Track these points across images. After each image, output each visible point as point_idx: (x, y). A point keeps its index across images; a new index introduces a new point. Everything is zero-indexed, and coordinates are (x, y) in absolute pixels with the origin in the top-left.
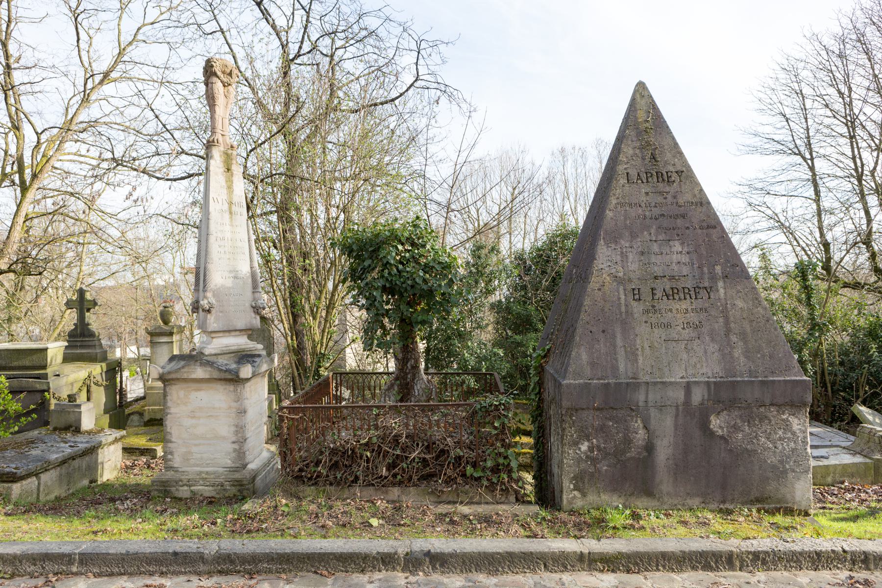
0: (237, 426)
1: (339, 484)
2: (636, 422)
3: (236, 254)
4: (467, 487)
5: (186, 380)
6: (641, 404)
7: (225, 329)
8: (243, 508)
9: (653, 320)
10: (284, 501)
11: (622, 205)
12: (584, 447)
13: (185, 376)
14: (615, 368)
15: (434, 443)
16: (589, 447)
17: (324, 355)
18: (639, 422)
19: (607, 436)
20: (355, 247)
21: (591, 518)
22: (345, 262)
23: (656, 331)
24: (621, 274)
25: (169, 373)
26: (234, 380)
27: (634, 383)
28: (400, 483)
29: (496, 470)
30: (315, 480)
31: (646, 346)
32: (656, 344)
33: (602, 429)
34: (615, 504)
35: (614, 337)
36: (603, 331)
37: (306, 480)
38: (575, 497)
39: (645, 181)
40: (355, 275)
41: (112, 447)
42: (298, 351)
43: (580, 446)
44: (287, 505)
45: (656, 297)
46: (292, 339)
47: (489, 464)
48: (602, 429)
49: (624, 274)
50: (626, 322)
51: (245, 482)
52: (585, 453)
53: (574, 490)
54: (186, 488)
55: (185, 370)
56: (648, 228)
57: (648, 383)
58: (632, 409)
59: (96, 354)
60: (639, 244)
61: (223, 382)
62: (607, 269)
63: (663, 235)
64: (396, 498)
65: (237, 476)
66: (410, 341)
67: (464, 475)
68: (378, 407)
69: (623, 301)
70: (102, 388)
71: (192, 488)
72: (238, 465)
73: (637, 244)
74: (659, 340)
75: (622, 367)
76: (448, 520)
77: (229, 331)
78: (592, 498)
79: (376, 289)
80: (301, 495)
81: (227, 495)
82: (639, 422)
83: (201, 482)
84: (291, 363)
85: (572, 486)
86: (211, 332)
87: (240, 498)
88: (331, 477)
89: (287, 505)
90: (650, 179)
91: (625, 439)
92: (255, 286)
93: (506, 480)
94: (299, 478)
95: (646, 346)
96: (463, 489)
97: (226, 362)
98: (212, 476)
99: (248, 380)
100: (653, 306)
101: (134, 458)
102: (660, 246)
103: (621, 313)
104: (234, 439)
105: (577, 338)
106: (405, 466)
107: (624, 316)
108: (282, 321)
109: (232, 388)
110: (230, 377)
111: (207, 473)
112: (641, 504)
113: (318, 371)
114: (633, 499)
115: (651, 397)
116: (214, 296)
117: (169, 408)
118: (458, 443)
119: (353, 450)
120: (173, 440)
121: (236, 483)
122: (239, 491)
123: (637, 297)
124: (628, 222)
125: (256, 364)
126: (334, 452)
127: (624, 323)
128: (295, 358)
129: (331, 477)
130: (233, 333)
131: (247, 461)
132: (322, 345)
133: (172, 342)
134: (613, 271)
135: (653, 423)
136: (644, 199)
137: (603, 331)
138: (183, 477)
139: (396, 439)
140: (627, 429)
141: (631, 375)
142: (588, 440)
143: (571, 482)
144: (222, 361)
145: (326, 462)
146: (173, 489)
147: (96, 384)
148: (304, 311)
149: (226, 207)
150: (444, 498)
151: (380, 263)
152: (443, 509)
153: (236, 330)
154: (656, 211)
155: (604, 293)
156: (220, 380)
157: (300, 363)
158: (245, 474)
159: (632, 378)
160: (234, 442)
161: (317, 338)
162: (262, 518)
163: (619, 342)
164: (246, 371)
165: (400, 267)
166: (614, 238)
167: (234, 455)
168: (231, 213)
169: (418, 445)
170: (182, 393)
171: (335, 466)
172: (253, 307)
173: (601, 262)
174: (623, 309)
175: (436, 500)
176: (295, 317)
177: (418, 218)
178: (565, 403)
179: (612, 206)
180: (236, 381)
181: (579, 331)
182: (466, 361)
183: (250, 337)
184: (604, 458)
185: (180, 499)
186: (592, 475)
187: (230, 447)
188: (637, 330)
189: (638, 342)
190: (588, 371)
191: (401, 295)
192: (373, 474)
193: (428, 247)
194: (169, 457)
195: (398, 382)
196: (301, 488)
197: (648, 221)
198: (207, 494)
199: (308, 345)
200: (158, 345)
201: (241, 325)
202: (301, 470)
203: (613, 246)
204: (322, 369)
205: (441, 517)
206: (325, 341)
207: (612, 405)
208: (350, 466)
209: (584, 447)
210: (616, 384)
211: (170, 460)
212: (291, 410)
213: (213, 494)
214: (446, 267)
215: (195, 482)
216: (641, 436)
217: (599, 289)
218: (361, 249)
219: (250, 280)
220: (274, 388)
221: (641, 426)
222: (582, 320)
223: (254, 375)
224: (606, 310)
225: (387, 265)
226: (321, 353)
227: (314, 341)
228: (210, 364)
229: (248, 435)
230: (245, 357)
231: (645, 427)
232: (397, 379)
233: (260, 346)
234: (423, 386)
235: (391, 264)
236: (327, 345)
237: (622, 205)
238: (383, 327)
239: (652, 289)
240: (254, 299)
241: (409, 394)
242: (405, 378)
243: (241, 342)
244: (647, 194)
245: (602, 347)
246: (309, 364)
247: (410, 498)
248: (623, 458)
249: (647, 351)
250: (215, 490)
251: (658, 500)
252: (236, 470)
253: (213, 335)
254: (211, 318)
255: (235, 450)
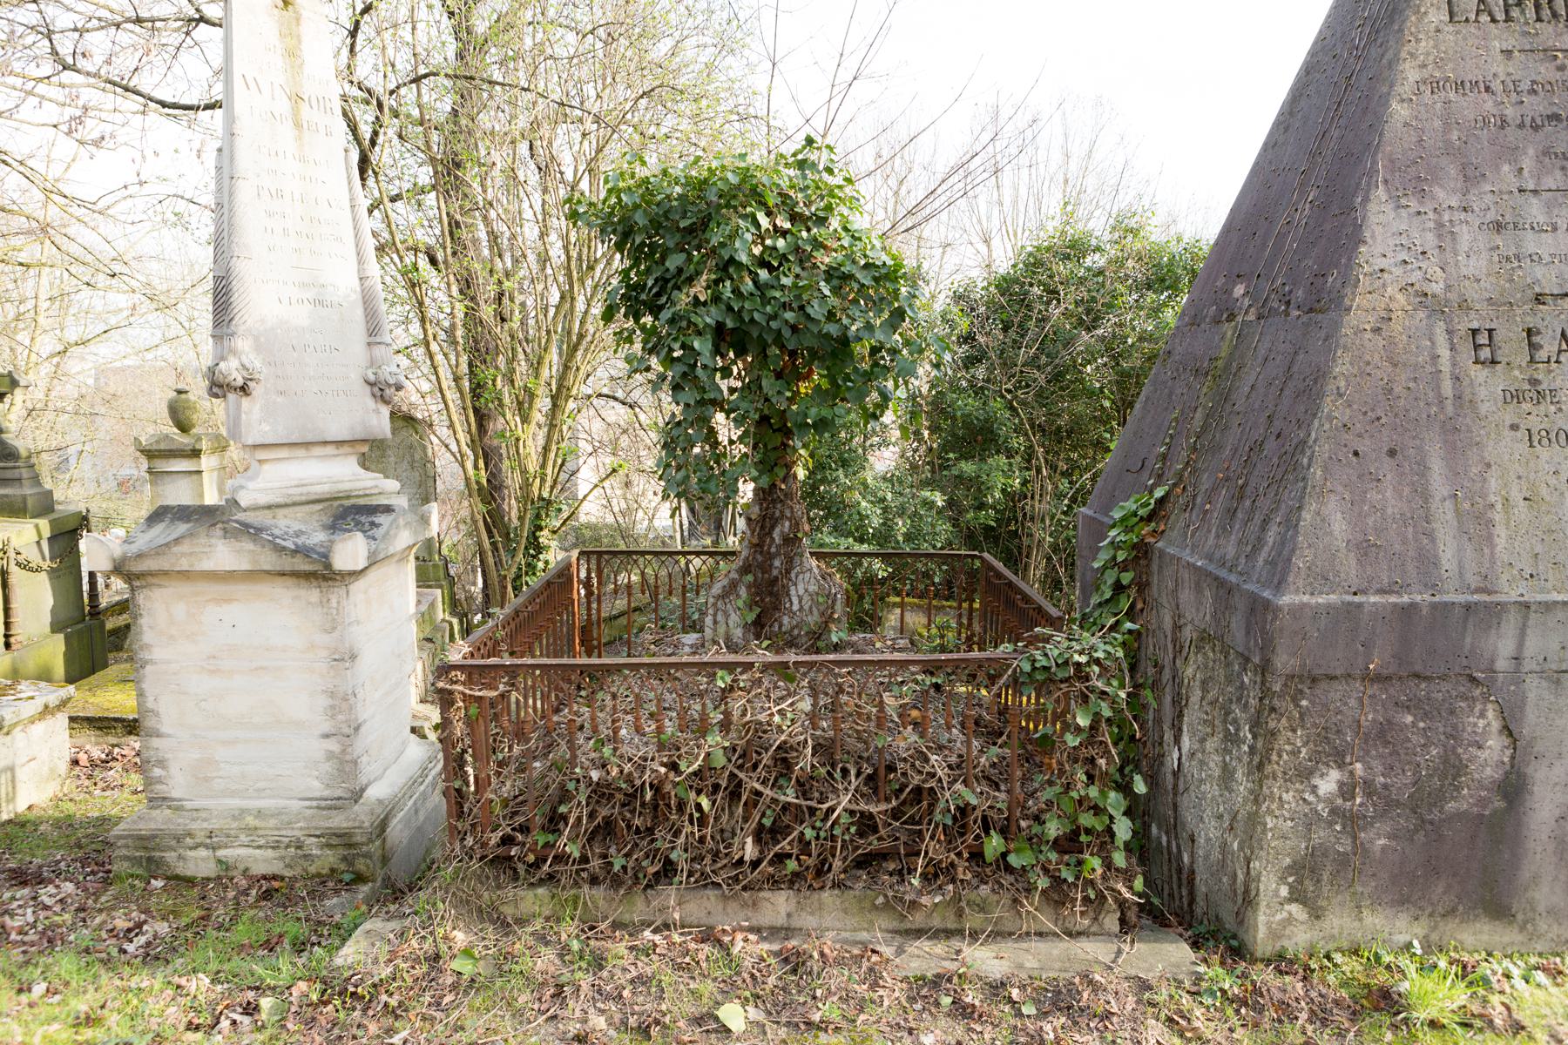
0: (332, 695)
1: (616, 882)
2: (1482, 715)
3: (323, 263)
4: (985, 890)
5: (186, 575)
6: (1502, 664)
7: (293, 439)
8: (339, 961)
9: (1535, 423)
10: (460, 937)
11: (1436, 86)
12: (1328, 783)
13: (184, 565)
14: (1427, 561)
15: (891, 768)
16: (1341, 784)
17: (549, 502)
18: (1490, 714)
19: (1395, 753)
20: (640, 219)
21: (1345, 984)
22: (611, 265)
23: (1544, 453)
24: (1437, 288)
25: (140, 556)
26: (320, 573)
27: (1486, 606)
28: (794, 879)
29: (1069, 844)
30: (544, 870)
31: (1516, 495)
32: (1544, 491)
33: (1384, 733)
34: (1402, 939)
35: (1423, 470)
36: (1392, 453)
37: (521, 868)
38: (1290, 920)
39: (1500, 16)
40: (636, 299)
41: (39, 728)
42: (490, 492)
43: (1316, 781)
44: (467, 953)
45: (1542, 355)
46: (476, 467)
47: (1053, 829)
48: (1384, 733)
49: (1448, 288)
50: (1456, 426)
51: (358, 839)
52: (1329, 801)
53: (1290, 900)
54: (203, 853)
55: (185, 547)
56: (1512, 153)
57: (1527, 606)
58: (1473, 679)
59: (24, 498)
60: (1489, 198)
61: (290, 581)
62: (1398, 271)
63: (1558, 174)
64: (781, 921)
65: (338, 821)
66: (781, 473)
67: (977, 856)
68: (729, 667)
69: (1445, 364)
70: (44, 575)
71: (221, 853)
72: (339, 793)
73: (1482, 198)
74: (1553, 481)
75: (1447, 555)
76: (946, 1001)
77: (307, 445)
78: (1340, 922)
79: (699, 333)
80: (508, 910)
81: (312, 870)
82: (1490, 714)
83: (243, 838)
84: (475, 522)
85: (1284, 891)
86: (256, 447)
87: (347, 877)
88: (595, 864)
89: (467, 953)
90: (1515, 13)
91: (1446, 761)
92: (373, 330)
93: (1099, 871)
94: (502, 863)
95: (1516, 495)
96: (973, 896)
97: (296, 526)
98: (272, 822)
99: (355, 574)
100: (1534, 382)
101: (113, 740)
102: (1549, 206)
103: (1441, 401)
104: (326, 727)
105: (1317, 472)
106: (809, 834)
107: (1450, 410)
108: (451, 426)
109: (312, 594)
110: (307, 567)
111: (259, 813)
112: (1473, 936)
113: (536, 539)
114: (1450, 926)
115: (1532, 645)
116: (258, 348)
117: (148, 646)
118: (959, 768)
119: (657, 788)
120: (164, 729)
121: (335, 841)
122: (344, 859)
123: (1485, 353)
124: (1455, 136)
125: (378, 532)
126: (601, 792)
127: (1450, 429)
128: (482, 508)
129: (595, 864)
130: (318, 451)
131: (364, 780)
132: (543, 481)
133: (199, 472)
134: (1416, 277)
135: (1531, 721)
136: (1501, 70)
137: (1392, 453)
138: (194, 826)
139: (784, 761)
140: (1454, 735)
141: (1474, 581)
142: (1341, 766)
143: (1283, 880)
144: (285, 524)
145: (579, 819)
146: (170, 856)
147: (25, 566)
148: (501, 405)
149: (283, 106)
150: (917, 920)
151: (711, 263)
152: (926, 957)
153: (325, 443)
154: (1536, 106)
155: (1391, 342)
156: (282, 574)
157: (494, 521)
158: (359, 817)
159: (1478, 590)
160: (327, 736)
161: (533, 466)
162: (393, 1002)
163: (1439, 484)
164: (350, 551)
165: (763, 274)
166: (1415, 182)
167: (327, 767)
168: (298, 125)
169: (845, 772)
170: (180, 610)
171: (606, 831)
172: (372, 384)
173: (1378, 250)
174: (1447, 388)
175: (895, 924)
176: (482, 418)
177: (810, 141)
178: (1284, 661)
179: (1405, 89)
180: (325, 578)
181: (1323, 450)
182: (862, 517)
183: (364, 462)
184: (1382, 815)
185: (190, 882)
186: (1343, 861)
187: (318, 748)
188: (1490, 452)
189: (1493, 484)
190: (1349, 567)
191: (763, 355)
192: (716, 855)
193: (835, 223)
194: (157, 772)
195: (750, 578)
196: (510, 892)
197: (1512, 134)
198: (259, 869)
199: (513, 480)
200: (167, 479)
201: (338, 428)
202: (507, 841)
203: (1414, 204)
204: (545, 532)
205: (928, 988)
206: (549, 471)
207: (1418, 668)
208: (650, 831)
209: (1328, 783)
210: (1434, 606)
211: (160, 781)
212: (474, 673)
213: (276, 868)
214: (887, 277)
215: (229, 839)
216: (1491, 754)
217: (1377, 330)
218: (656, 225)
219: (359, 312)
220: (431, 569)
221: (1496, 725)
222: (1330, 418)
223: (373, 561)
224: (1398, 389)
225: (728, 266)
226: (541, 498)
227: (524, 471)
228: (251, 531)
229: (363, 714)
230: (351, 514)
231: (1507, 730)
232: (745, 570)
233: (392, 485)
234: (812, 588)
235: (739, 265)
236: (555, 482)
237: (1436, 86)
238: (711, 436)
239: (1529, 332)
240: (372, 363)
241: (777, 608)
242: (765, 567)
243: (343, 474)
244: (1507, 53)
245: (1389, 498)
246: (515, 523)
247: (830, 921)
248: (1436, 815)
249: (1521, 510)
250: (282, 858)
251: (1522, 928)
252: (334, 805)
253: (262, 455)
254: (251, 409)
255: (330, 756)
